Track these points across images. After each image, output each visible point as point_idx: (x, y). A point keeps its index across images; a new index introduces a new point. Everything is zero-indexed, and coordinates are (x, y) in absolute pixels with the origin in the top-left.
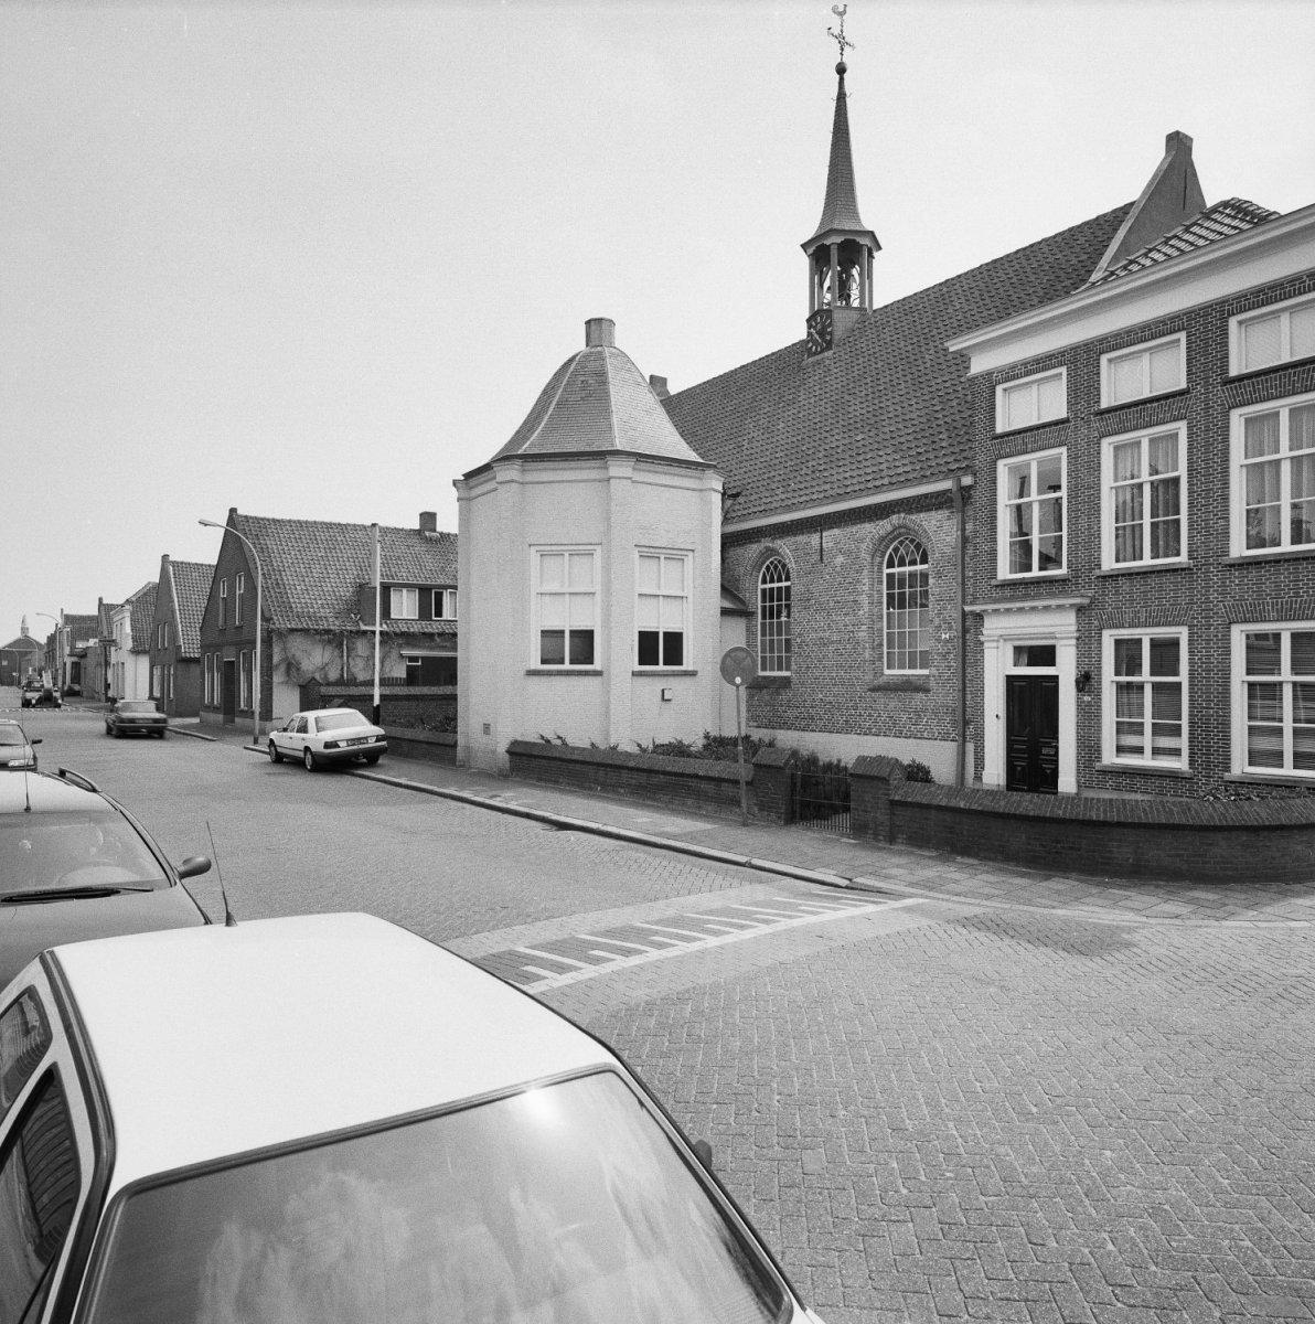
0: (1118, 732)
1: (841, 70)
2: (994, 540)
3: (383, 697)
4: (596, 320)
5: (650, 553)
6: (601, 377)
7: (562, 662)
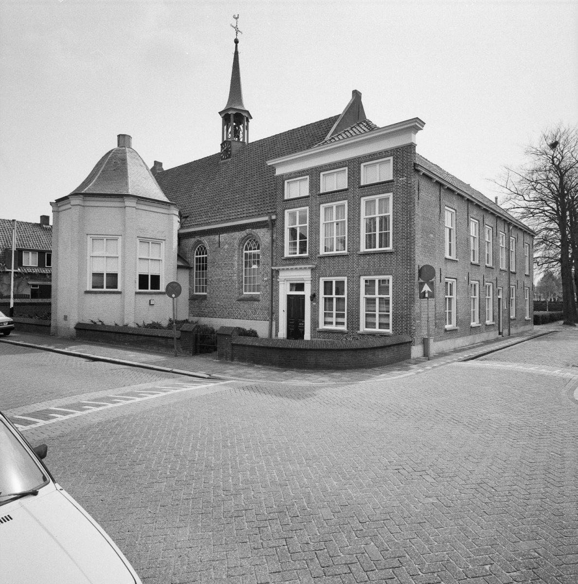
0: (325, 316)
1: (236, 42)
2: (283, 242)
3: (15, 304)
4: (122, 135)
5: (144, 240)
6: (124, 161)
7: (102, 287)
